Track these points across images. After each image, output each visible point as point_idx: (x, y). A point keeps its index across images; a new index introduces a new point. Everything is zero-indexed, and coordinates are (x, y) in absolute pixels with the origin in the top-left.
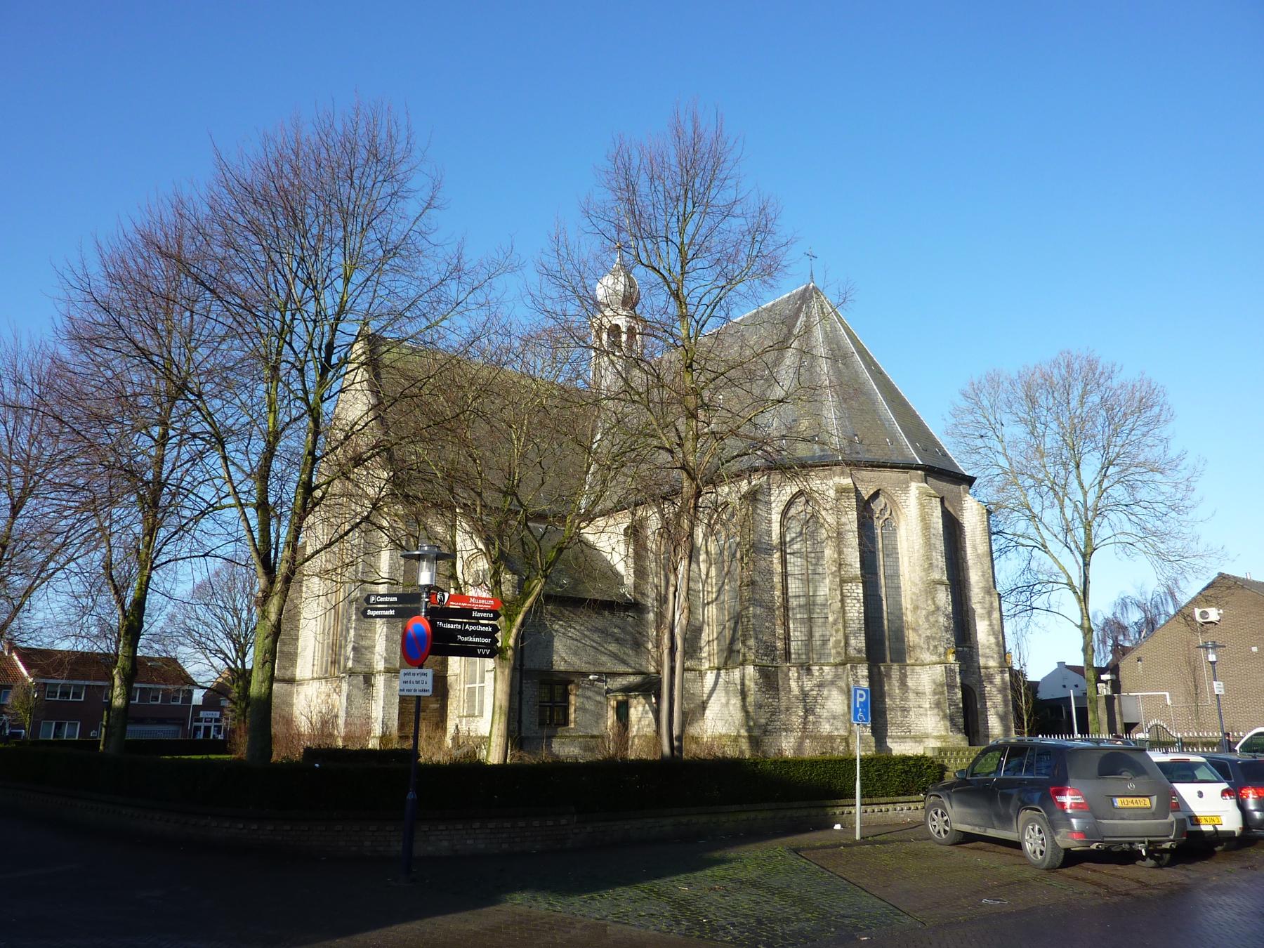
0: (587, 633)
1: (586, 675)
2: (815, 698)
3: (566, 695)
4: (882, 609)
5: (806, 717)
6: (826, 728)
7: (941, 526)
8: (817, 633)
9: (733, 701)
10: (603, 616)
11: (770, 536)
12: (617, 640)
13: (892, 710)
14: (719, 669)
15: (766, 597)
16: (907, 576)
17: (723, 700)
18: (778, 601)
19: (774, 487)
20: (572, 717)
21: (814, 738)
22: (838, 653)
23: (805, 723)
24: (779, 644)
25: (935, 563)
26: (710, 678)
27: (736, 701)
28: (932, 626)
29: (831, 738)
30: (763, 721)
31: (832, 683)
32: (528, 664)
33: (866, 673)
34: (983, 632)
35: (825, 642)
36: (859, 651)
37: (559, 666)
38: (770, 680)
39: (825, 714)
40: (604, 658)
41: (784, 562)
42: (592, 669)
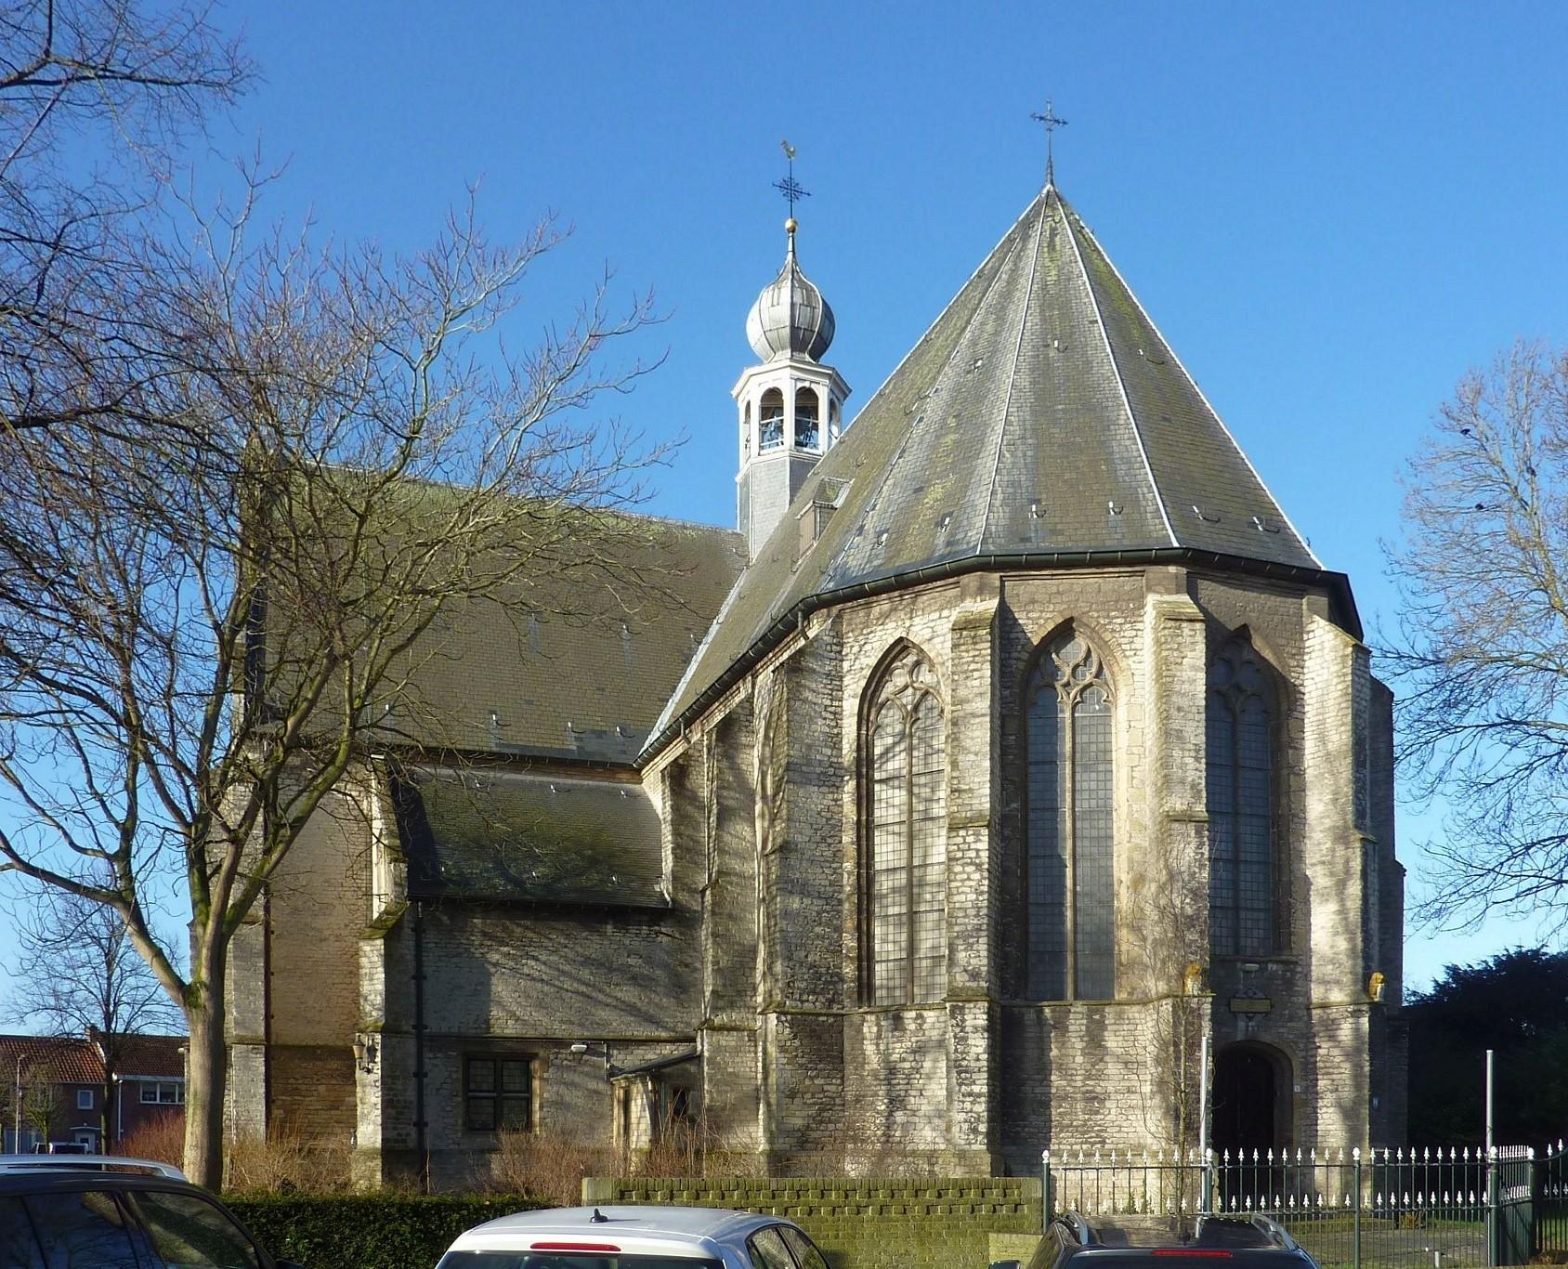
0: (567, 968)
1: (563, 1043)
2: (908, 1077)
3: (529, 1077)
5: (891, 1114)
6: (927, 1136)
7: (1201, 688)
10: (603, 934)
12: (635, 979)
13: (1065, 1098)
18: (848, 883)
20: (536, 1117)
24: (849, 970)
25: (1177, 773)
32: (434, 1025)
33: (982, 1020)
36: (974, 976)
39: (925, 1108)
40: (603, 1014)
42: (578, 1032)
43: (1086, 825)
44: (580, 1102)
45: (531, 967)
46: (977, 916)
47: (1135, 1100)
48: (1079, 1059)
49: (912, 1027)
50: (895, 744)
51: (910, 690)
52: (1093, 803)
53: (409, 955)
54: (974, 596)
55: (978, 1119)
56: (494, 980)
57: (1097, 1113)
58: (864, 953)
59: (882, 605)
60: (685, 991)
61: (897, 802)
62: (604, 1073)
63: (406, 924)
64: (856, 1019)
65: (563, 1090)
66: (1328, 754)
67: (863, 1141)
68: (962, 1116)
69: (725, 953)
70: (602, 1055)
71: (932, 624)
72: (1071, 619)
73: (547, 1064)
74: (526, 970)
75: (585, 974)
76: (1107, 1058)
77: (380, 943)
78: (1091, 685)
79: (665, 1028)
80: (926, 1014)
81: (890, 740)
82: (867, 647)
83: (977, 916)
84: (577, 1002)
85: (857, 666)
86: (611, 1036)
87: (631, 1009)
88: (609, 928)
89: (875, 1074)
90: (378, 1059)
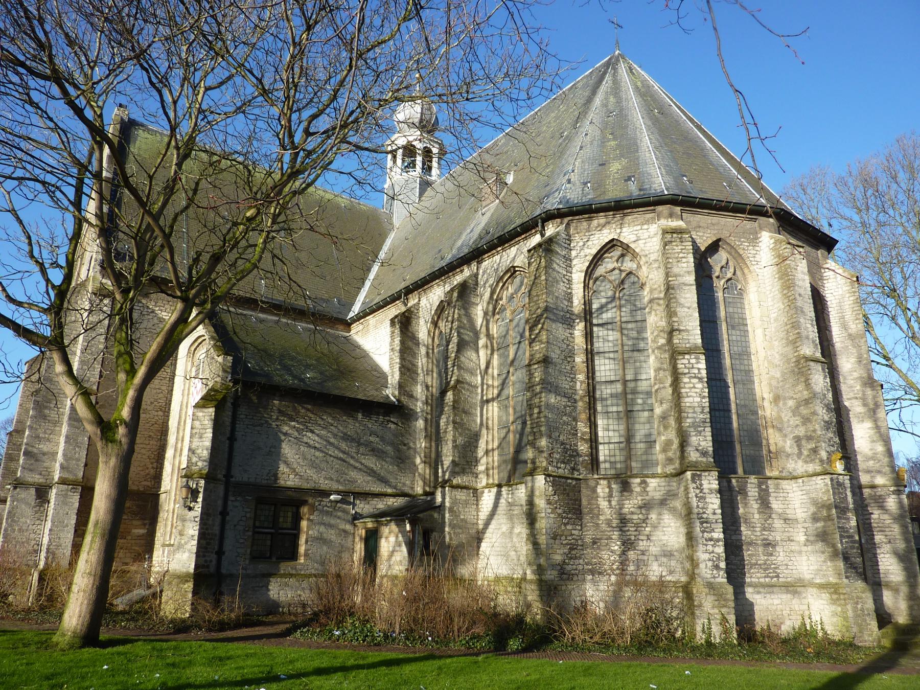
0: (332, 440)
1: (326, 494)
2: (637, 526)
3: (297, 519)
4: (728, 399)
5: (624, 553)
6: (655, 571)
8: (641, 431)
9: (518, 529)
11: (570, 300)
13: (750, 544)
14: (499, 486)
15: (565, 385)
16: (762, 354)
17: (504, 528)
18: (580, 388)
19: (577, 238)
20: (302, 549)
21: (637, 585)
22: (670, 460)
23: (623, 563)
24: (583, 448)
25: (804, 333)
26: (487, 499)
27: (521, 530)
28: (806, 420)
29: (662, 585)
30: (558, 558)
31: (663, 503)
32: (238, 476)
33: (715, 485)
34: (862, 436)
35: (651, 443)
36: (704, 454)
37: (288, 478)
38: (571, 500)
39: (654, 550)
40: (353, 474)
41: (589, 336)
42: (336, 486)
43: (738, 362)
44: (333, 538)
45: (310, 438)
46: (702, 412)
47: (794, 547)
48: (757, 516)
49: (638, 489)
50: (607, 303)
51: (617, 271)
52: (740, 349)
53: (228, 420)
54: (666, 218)
55: (718, 559)
56: (284, 445)
57: (771, 555)
58: (593, 437)
59: (601, 219)
60: (403, 462)
61: (611, 338)
62: (350, 518)
63: (229, 399)
64: (592, 483)
65: (322, 529)
66: (850, 335)
67: (600, 573)
68: (707, 556)
69: (460, 435)
70: (349, 503)
71: (644, 234)
72: (719, 240)
73: (313, 509)
74: (305, 439)
75: (343, 446)
76: (774, 516)
77: (212, 410)
78: (730, 279)
79: (390, 486)
80: (648, 480)
81: (604, 301)
82: (590, 243)
83: (702, 412)
84: (337, 464)
85: (582, 254)
86: (357, 490)
87: (371, 472)
88: (360, 416)
89: (609, 523)
90: (200, 500)
